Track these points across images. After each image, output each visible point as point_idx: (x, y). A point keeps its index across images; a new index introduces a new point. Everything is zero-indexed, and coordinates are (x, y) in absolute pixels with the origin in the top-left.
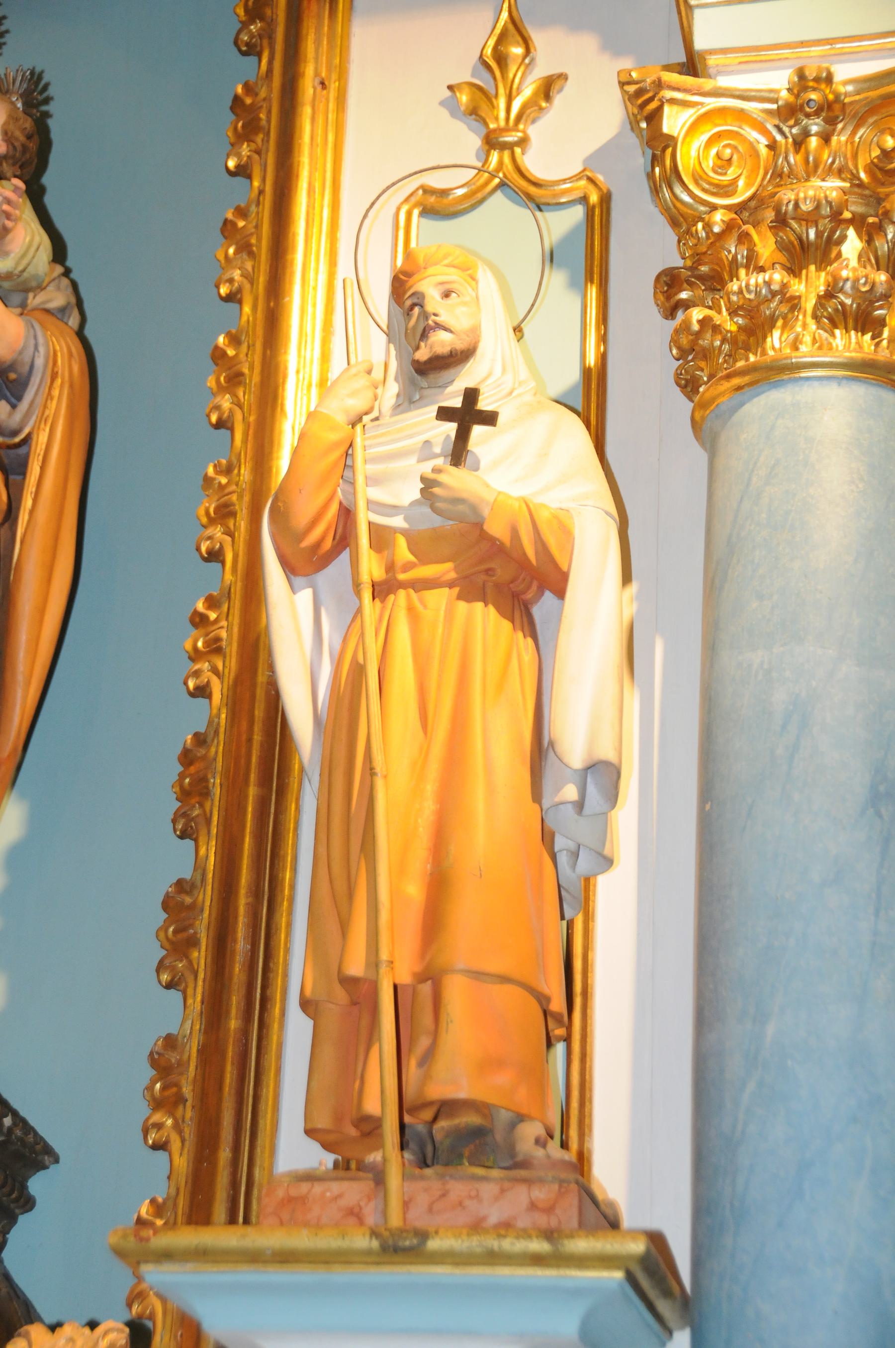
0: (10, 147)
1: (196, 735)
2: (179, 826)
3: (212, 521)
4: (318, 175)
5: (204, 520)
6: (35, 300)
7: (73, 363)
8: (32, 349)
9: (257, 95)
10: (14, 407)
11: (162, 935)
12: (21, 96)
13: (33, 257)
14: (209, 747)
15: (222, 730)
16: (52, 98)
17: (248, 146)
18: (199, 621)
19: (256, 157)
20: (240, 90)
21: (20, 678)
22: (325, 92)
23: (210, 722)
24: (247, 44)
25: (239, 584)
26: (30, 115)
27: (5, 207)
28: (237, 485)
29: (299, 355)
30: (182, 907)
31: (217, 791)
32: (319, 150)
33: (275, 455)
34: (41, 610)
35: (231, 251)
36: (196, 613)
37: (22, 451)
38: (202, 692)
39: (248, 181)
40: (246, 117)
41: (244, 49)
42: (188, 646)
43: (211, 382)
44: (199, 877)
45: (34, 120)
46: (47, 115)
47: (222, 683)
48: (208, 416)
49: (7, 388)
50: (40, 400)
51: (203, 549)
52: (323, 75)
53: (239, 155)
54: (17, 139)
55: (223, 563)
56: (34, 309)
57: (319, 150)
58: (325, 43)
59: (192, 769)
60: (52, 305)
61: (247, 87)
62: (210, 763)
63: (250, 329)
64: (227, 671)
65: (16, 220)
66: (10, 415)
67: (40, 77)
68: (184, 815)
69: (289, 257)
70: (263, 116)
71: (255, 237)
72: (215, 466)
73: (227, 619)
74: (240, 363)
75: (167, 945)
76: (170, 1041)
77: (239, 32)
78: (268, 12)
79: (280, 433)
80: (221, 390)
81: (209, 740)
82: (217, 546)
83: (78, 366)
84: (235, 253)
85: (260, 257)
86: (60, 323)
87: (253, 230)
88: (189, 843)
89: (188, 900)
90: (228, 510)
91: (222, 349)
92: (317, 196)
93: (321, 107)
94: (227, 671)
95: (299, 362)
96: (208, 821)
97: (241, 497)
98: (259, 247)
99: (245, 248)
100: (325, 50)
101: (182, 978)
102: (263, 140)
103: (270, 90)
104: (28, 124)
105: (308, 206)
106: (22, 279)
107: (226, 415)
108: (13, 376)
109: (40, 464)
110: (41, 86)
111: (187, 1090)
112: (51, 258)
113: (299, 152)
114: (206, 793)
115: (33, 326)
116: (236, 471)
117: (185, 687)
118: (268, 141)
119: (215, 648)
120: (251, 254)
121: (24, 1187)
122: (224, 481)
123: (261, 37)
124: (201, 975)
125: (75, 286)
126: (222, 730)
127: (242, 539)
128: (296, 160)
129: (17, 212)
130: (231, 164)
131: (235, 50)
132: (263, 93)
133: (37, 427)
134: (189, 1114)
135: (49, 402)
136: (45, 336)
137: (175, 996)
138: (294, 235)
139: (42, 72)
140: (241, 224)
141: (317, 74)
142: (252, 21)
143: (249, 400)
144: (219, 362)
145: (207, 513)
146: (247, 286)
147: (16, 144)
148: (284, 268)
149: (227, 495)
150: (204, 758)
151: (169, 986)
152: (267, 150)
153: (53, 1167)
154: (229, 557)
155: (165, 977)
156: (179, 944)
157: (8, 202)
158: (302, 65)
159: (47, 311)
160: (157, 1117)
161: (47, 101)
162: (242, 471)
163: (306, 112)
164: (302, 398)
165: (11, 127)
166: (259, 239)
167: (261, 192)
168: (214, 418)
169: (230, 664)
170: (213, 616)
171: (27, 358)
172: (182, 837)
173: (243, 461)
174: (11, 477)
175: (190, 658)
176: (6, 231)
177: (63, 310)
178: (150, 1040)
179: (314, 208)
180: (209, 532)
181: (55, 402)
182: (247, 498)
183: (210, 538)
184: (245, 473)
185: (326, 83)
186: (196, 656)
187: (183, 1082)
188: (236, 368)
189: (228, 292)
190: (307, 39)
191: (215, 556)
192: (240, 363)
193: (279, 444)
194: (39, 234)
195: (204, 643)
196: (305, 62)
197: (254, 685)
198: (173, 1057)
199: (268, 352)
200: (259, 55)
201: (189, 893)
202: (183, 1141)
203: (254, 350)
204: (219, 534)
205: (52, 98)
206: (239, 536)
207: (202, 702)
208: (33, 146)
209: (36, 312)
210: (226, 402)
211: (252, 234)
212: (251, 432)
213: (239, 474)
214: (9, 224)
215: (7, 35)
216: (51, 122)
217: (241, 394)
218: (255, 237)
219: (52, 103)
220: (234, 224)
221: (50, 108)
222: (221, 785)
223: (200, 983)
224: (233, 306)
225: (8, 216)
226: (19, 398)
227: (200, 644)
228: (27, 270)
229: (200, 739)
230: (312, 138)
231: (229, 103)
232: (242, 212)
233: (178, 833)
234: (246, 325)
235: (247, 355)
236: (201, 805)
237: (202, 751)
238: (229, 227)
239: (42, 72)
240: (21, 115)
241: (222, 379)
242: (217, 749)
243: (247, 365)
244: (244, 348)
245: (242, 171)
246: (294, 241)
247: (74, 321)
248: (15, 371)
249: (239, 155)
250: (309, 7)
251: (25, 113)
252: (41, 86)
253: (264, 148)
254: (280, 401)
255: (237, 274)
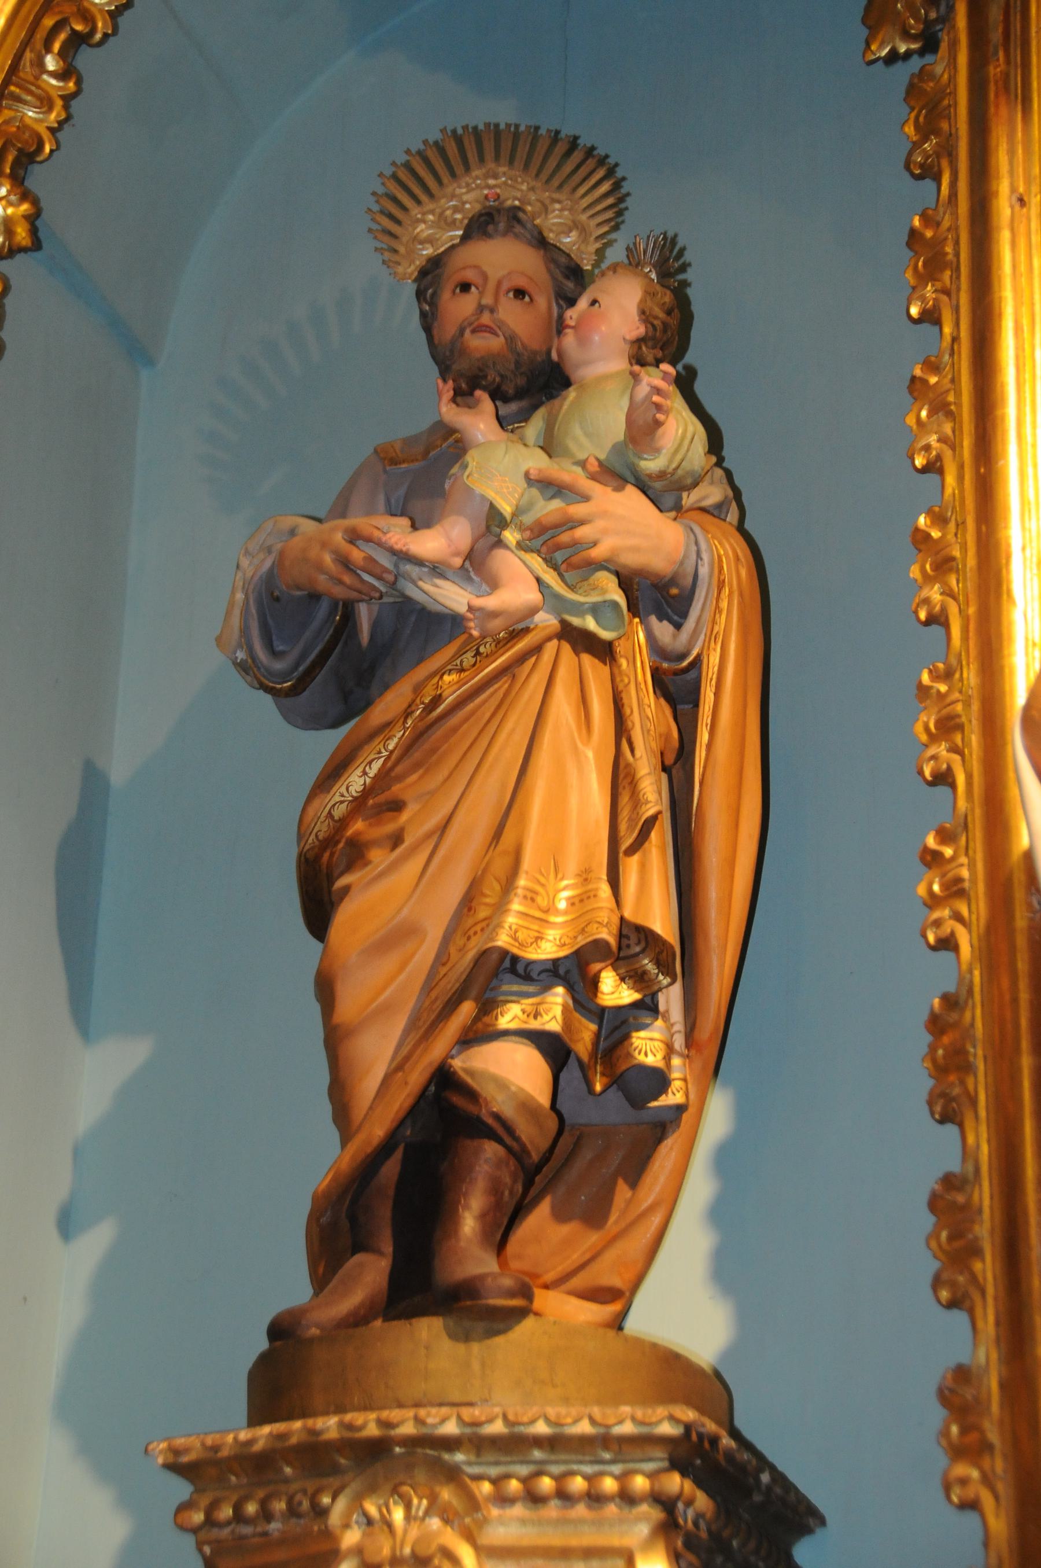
0: (649, 326)
1: (946, 998)
2: (938, 1108)
3: (933, 738)
4: (1025, 310)
5: (924, 738)
6: (688, 499)
7: (740, 567)
8: (694, 556)
9: (938, 224)
10: (678, 626)
11: (934, 1244)
12: (654, 266)
13: (688, 450)
14: (963, 1010)
15: (977, 989)
16: (690, 265)
17: (933, 286)
18: (932, 859)
19: (944, 298)
20: (916, 222)
21: (714, 942)
22: (1025, 210)
23: (961, 980)
24: (922, 166)
25: (978, 812)
26: (668, 287)
27: (656, 398)
28: (961, 692)
29: (1023, 528)
30: (954, 1207)
31: (981, 1066)
32: (1024, 280)
33: (1006, 652)
34: (731, 863)
35: (924, 414)
36: (926, 850)
37: (692, 675)
38: (947, 944)
39: (937, 328)
40: (928, 255)
41: (918, 172)
42: (921, 890)
43: (915, 572)
44: (970, 1168)
45: (671, 290)
46: (685, 284)
47: (970, 932)
48: (916, 613)
49: (669, 606)
50: (707, 616)
51: (927, 773)
52: (1021, 190)
53: (923, 299)
54: (656, 318)
55: (953, 786)
56: (687, 511)
57: (1024, 280)
58: (1020, 151)
59: (946, 1040)
60: (708, 503)
61: (924, 216)
62: (968, 1033)
63: (957, 504)
64: (974, 917)
65: (667, 413)
66: (675, 637)
67: (674, 241)
68: (943, 1095)
69: (999, 413)
70: (949, 249)
71: (952, 393)
72: (930, 671)
73: (967, 854)
74: (950, 545)
75: (940, 1254)
76: (962, 1374)
77: (910, 154)
78: (945, 126)
79: (1010, 624)
80: (928, 580)
81: (962, 1000)
82: (945, 766)
83: (745, 571)
84: (929, 416)
85: (961, 416)
86: (716, 520)
87: (949, 386)
88: (952, 1129)
89: (960, 1199)
90: (952, 723)
91: (923, 531)
92: (1026, 334)
93: (1022, 229)
94: (974, 917)
95: (1024, 537)
96: (974, 1102)
97: (967, 704)
98: (959, 405)
99: (941, 408)
100: (1021, 160)
101: (966, 1295)
102: (951, 277)
103: (955, 215)
104: (668, 298)
105: (1017, 348)
106: (676, 477)
107: (938, 608)
108: (674, 591)
109: (713, 689)
110: (675, 253)
111: (993, 1436)
112: (707, 449)
113: (1000, 287)
114: (967, 1068)
115: (692, 530)
116: (957, 676)
117: (922, 940)
118: (958, 277)
119: (955, 889)
120: (950, 415)
121: (789, 1557)
122: (943, 688)
123: (938, 155)
124: (990, 1290)
125: (729, 475)
126: (977, 989)
127: (974, 757)
128: (996, 296)
129: (669, 402)
130: (914, 311)
131: (907, 175)
132: (946, 223)
133: (706, 646)
134: (999, 1465)
135: (717, 616)
136: (708, 541)
137: (960, 1318)
138: (1003, 385)
139: (676, 236)
140: (933, 380)
141: (1013, 189)
142: (925, 139)
143: (965, 587)
144: (922, 547)
145: (927, 729)
146: (948, 454)
147: (656, 322)
148: (994, 426)
149: (949, 705)
150: (956, 1025)
151: (953, 1304)
152: (959, 289)
153: (820, 1533)
154: (961, 779)
155: (944, 1294)
156: (958, 1253)
157: (658, 391)
158: (994, 183)
159: (703, 510)
160: (961, 1469)
161: (683, 268)
162: (965, 675)
163: (1004, 237)
164: (1032, 579)
165: (649, 303)
166: (958, 394)
167: (955, 339)
168: (923, 615)
169: (977, 908)
170: (948, 852)
171: (690, 569)
172: (942, 1122)
173: (964, 663)
174: (679, 707)
175: (925, 904)
176: (658, 424)
177: (719, 506)
178: (934, 1372)
179: (1024, 350)
180: (932, 751)
181: (724, 616)
182: (976, 706)
183: (934, 757)
184: (971, 676)
185: (1026, 199)
186: (933, 901)
187: (987, 1425)
188: (943, 553)
189: (925, 462)
190: (997, 151)
191: (943, 779)
192: (950, 545)
193: (1010, 639)
194: (692, 423)
195: (942, 885)
196: (998, 178)
197: (1011, 932)
198: (969, 1393)
199: (984, 528)
200: (937, 179)
201: (960, 1189)
202: (997, 1497)
203: (965, 530)
204: (944, 753)
205: (690, 265)
206: (971, 754)
207: (947, 956)
208: (673, 322)
209: (692, 512)
210: (935, 594)
211: (948, 391)
212: (972, 627)
213: (961, 679)
214: (660, 417)
215: (628, 199)
216: (690, 291)
217: (953, 582)
218: (952, 393)
219: (689, 270)
220: (925, 382)
221: (689, 275)
222: (985, 1057)
223: (990, 1301)
224: (933, 478)
225: (658, 407)
226: (685, 615)
227: (936, 888)
228: (682, 466)
229: (950, 1002)
230: (1014, 267)
231: (905, 238)
232: (932, 366)
233: (937, 1116)
234: (951, 499)
235: (956, 535)
236: (963, 1083)
237: (954, 1016)
238: (918, 385)
239: (676, 236)
240: (659, 288)
241: (928, 567)
242: (976, 1016)
243: (958, 547)
244: (952, 526)
245: (931, 317)
246: (1003, 392)
247: (733, 516)
248: (677, 585)
249: (923, 299)
250: (997, 113)
251: (663, 286)
252: (675, 253)
253: (954, 287)
254: (1005, 588)
255: (933, 439)
